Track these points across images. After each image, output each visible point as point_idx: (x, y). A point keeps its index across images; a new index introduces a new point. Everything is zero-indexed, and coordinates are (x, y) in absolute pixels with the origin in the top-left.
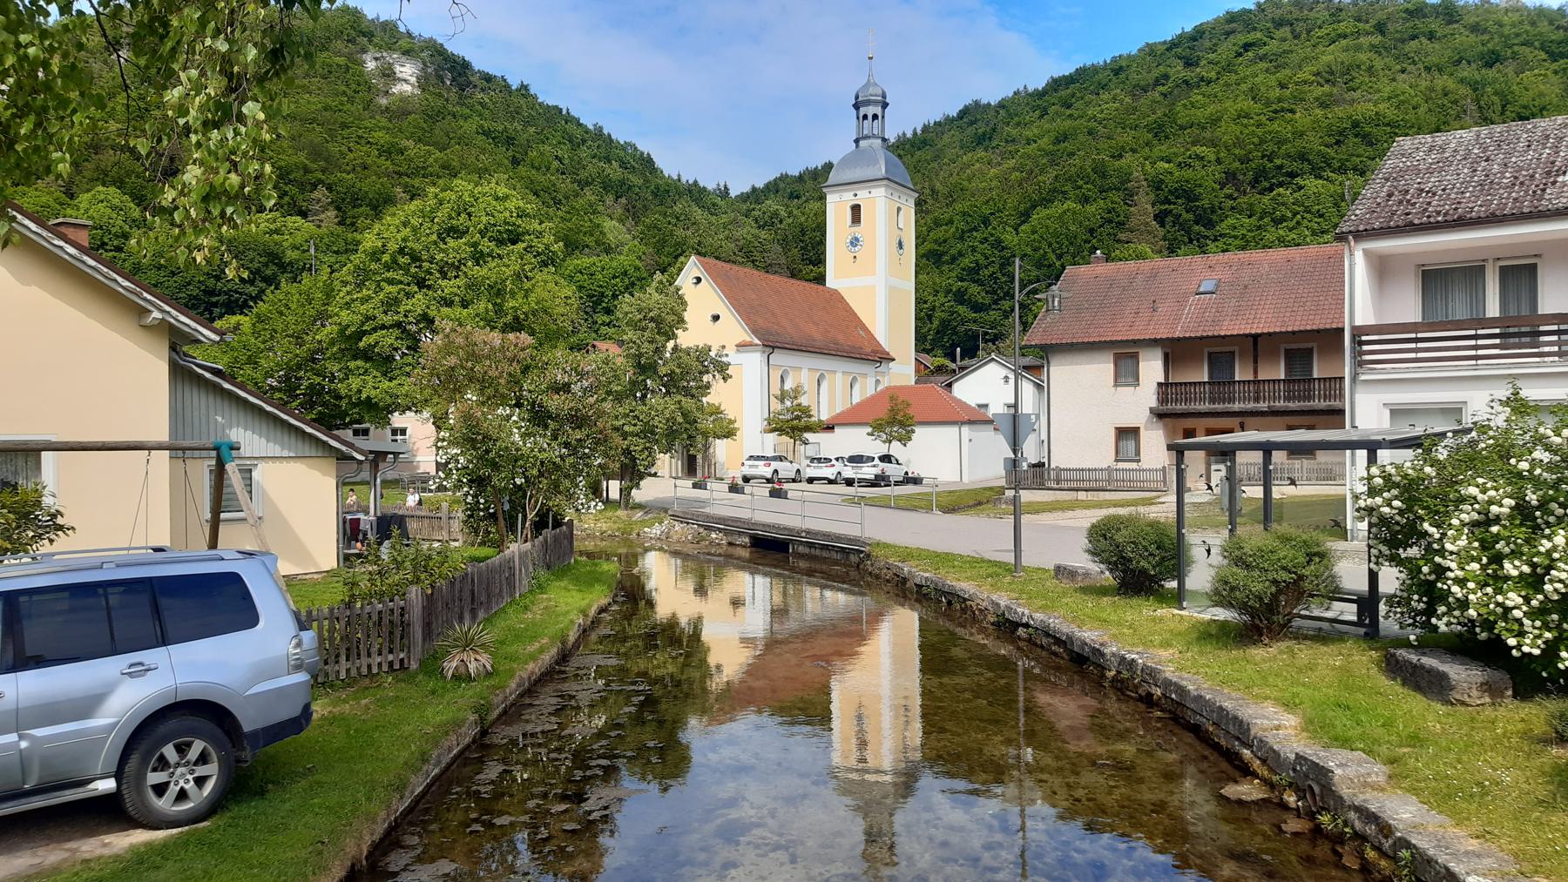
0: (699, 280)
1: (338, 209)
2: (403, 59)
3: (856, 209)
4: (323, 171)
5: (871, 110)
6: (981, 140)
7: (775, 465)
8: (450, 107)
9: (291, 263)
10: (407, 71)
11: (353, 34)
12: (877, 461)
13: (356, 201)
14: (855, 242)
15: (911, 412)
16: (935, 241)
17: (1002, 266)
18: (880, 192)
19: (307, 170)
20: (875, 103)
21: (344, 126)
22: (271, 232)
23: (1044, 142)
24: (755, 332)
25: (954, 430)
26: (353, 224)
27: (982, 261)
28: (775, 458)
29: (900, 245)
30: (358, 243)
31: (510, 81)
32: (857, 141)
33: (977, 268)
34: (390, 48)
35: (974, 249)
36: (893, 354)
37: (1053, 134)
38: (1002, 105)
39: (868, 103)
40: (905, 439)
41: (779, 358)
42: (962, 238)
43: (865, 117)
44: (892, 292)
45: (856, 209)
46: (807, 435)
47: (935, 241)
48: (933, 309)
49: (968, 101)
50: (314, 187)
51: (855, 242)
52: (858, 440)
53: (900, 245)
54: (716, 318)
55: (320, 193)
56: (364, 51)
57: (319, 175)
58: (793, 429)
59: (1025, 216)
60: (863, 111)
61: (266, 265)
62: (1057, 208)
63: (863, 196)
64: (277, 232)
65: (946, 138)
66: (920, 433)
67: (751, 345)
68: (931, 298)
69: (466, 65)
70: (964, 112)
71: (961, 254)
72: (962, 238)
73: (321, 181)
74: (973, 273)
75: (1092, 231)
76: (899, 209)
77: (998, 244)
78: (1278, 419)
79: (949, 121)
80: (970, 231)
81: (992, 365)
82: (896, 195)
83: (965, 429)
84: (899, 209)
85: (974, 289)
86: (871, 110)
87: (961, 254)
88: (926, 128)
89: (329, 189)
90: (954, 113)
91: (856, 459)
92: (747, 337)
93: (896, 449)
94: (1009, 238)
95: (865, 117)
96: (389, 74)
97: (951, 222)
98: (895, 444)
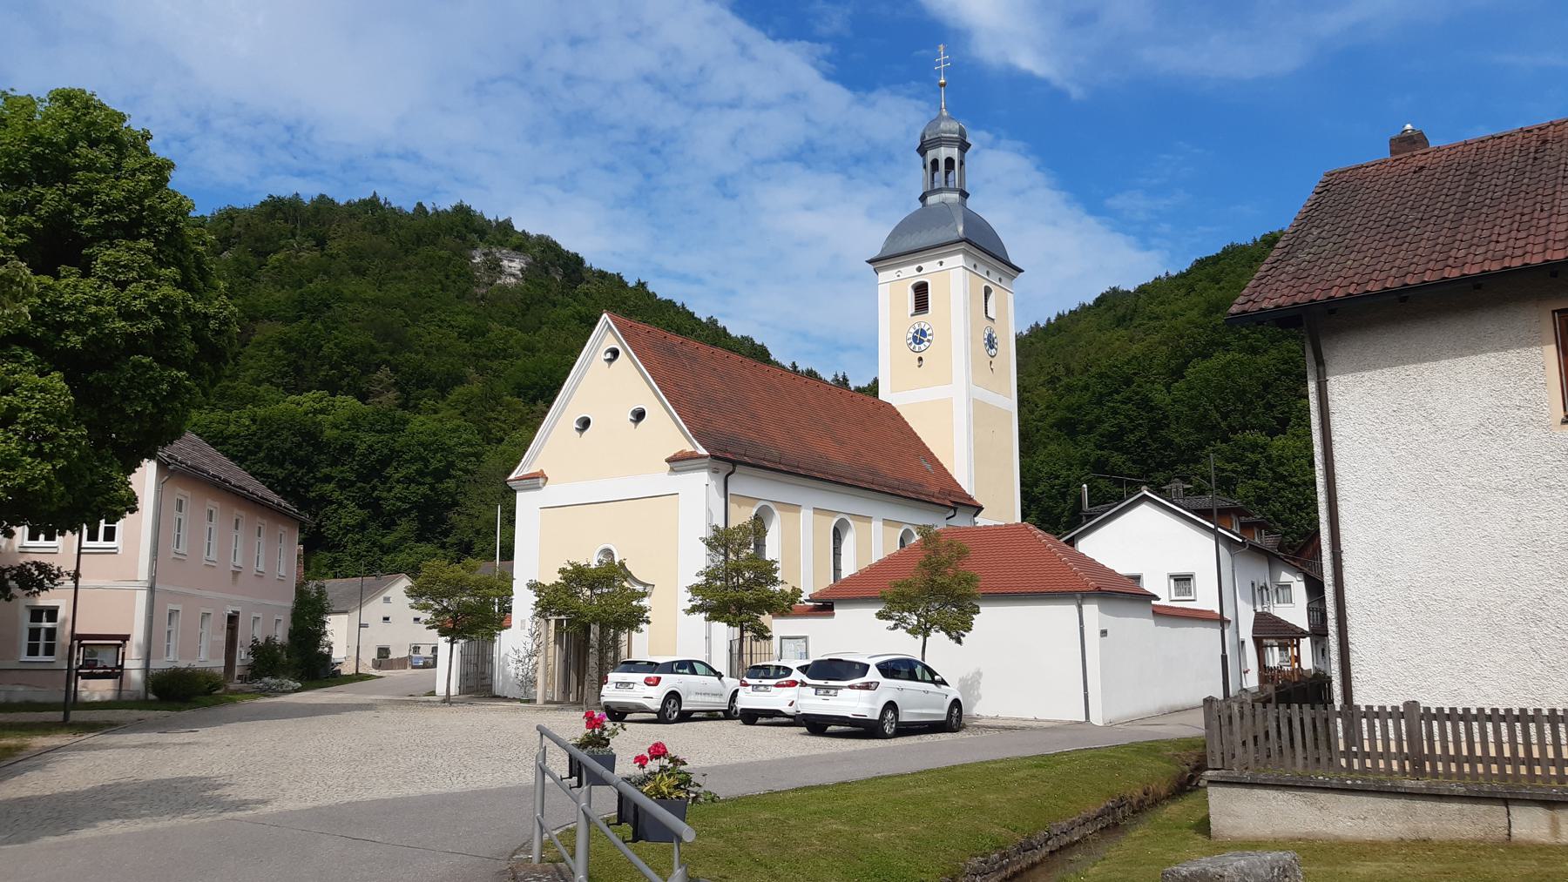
0: (615, 353)
1: (402, 390)
2: (513, 254)
3: (921, 290)
4: (391, 353)
5: (943, 153)
6: (1121, 321)
7: (669, 682)
8: (551, 296)
9: (328, 444)
10: (514, 265)
11: (464, 230)
12: (873, 675)
13: (423, 381)
14: (920, 337)
15: (968, 567)
16: (1068, 408)
17: (1152, 431)
18: (956, 262)
19: (374, 351)
20: (949, 142)
21: (431, 310)
22: (315, 412)
23: (1194, 314)
24: (699, 436)
25: (1068, 611)
26: (415, 406)
27: (1126, 423)
28: (670, 668)
29: (991, 342)
30: (407, 422)
31: (626, 279)
32: (923, 198)
33: (1122, 431)
34: (501, 244)
35: (1115, 412)
36: (979, 500)
37: (1204, 306)
38: (1142, 289)
39: (938, 142)
40: (957, 629)
41: (743, 485)
42: (1100, 403)
43: (935, 163)
44: (980, 412)
45: (921, 290)
46: (766, 619)
47: (1068, 408)
48: (1067, 486)
49: (1105, 289)
50: (378, 367)
51: (920, 337)
52: (862, 634)
53: (991, 342)
54: (639, 415)
55: (384, 374)
56: (474, 247)
57: (386, 356)
58: (741, 606)
59: (1178, 374)
60: (931, 155)
61: (299, 446)
62: (1220, 359)
63: (931, 270)
64: (323, 411)
65: (1082, 325)
66: (990, 619)
67: (693, 457)
68: (1064, 473)
69: (577, 261)
70: (1100, 300)
71: (1099, 420)
72: (1100, 403)
73: (387, 363)
74: (1114, 440)
75: (1266, 386)
76: (987, 291)
77: (1146, 404)
78: (1008, 723)
79: (1084, 308)
80: (1110, 394)
81: (1144, 510)
82: (982, 271)
83: (1091, 610)
84: (987, 291)
85: (1117, 458)
86: (943, 153)
87: (1099, 420)
88: (1060, 317)
89: (395, 369)
90: (1090, 301)
91: (831, 671)
92: (682, 442)
93: (939, 650)
94: (1160, 396)
95: (935, 163)
96: (495, 267)
97: (1086, 388)
98: (938, 638)
